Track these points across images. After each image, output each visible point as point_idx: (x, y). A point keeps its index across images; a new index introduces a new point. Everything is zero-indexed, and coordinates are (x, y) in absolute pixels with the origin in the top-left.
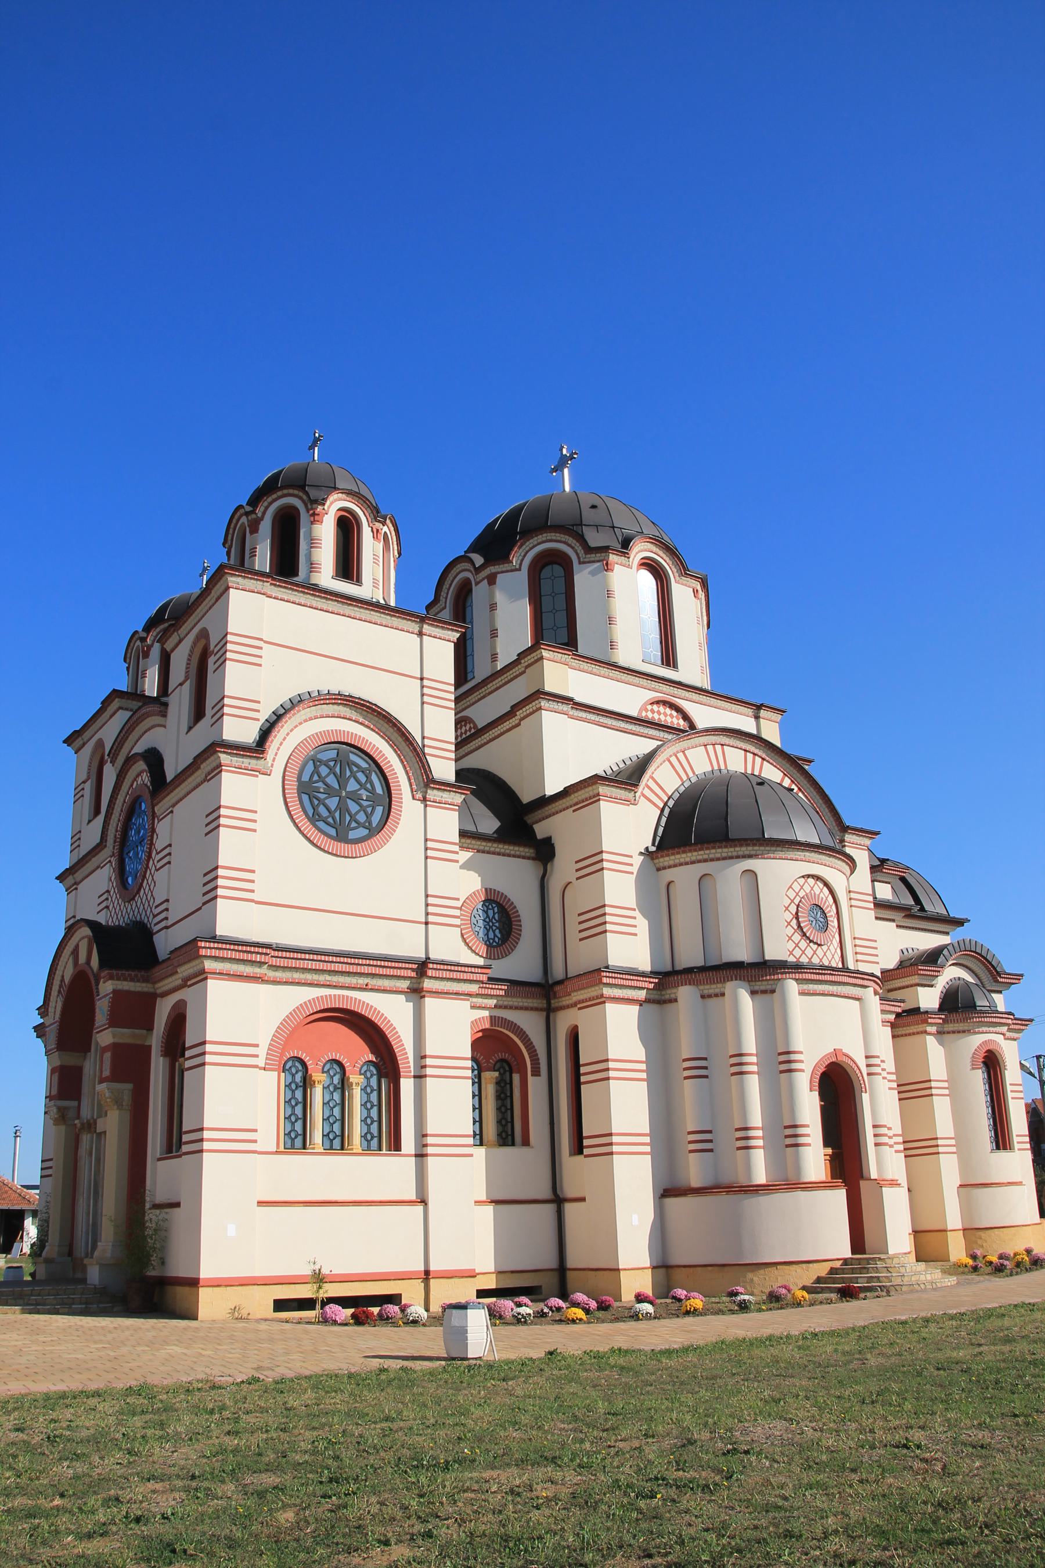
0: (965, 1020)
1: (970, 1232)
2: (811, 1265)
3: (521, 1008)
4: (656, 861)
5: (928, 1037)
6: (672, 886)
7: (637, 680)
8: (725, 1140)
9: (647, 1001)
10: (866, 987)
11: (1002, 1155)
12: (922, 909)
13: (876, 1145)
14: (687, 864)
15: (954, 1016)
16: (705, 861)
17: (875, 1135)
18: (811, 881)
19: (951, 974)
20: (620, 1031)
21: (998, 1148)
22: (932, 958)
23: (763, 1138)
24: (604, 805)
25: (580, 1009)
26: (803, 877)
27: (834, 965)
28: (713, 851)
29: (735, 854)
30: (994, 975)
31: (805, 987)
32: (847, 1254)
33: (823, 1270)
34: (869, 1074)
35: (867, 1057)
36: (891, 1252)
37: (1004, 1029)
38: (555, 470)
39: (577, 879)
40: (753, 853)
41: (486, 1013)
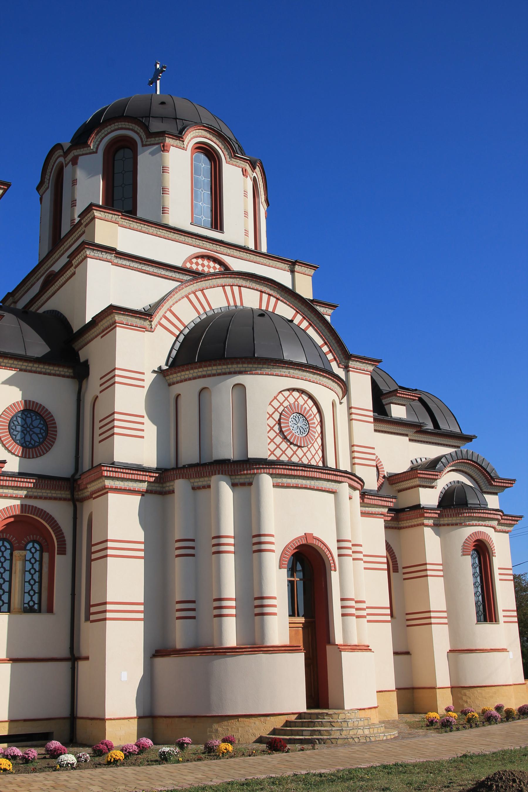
0: (457, 515)
1: (458, 690)
2: (268, 718)
3: (50, 498)
4: (167, 378)
5: (426, 529)
6: (179, 397)
7: (182, 238)
8: (205, 609)
9: (147, 491)
10: (340, 482)
11: (488, 627)
12: (436, 425)
13: (343, 615)
14: (190, 379)
15: (448, 512)
16: (204, 376)
17: (342, 607)
18: (296, 394)
19: (448, 478)
20: (122, 516)
21: (485, 620)
22: (434, 466)
23: (236, 607)
24: (120, 331)
25: (94, 498)
26: (288, 390)
27: (313, 463)
28: (210, 368)
29: (228, 370)
30: (488, 479)
31: (279, 480)
32: (302, 708)
33: (278, 723)
34: (339, 555)
35: (338, 541)
36: (348, 706)
37: (495, 523)
38: (151, 83)
39: (101, 392)
40: (242, 369)
41: (18, 502)
